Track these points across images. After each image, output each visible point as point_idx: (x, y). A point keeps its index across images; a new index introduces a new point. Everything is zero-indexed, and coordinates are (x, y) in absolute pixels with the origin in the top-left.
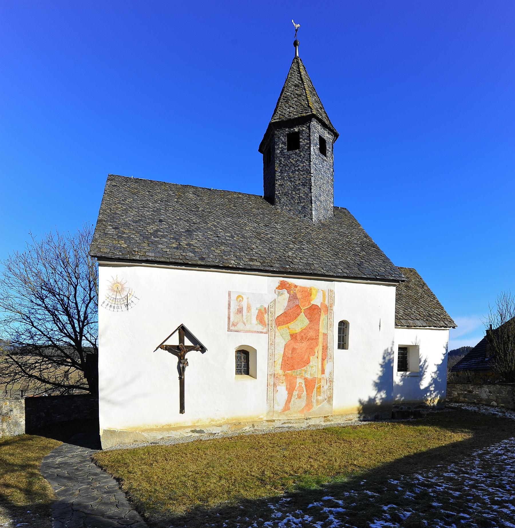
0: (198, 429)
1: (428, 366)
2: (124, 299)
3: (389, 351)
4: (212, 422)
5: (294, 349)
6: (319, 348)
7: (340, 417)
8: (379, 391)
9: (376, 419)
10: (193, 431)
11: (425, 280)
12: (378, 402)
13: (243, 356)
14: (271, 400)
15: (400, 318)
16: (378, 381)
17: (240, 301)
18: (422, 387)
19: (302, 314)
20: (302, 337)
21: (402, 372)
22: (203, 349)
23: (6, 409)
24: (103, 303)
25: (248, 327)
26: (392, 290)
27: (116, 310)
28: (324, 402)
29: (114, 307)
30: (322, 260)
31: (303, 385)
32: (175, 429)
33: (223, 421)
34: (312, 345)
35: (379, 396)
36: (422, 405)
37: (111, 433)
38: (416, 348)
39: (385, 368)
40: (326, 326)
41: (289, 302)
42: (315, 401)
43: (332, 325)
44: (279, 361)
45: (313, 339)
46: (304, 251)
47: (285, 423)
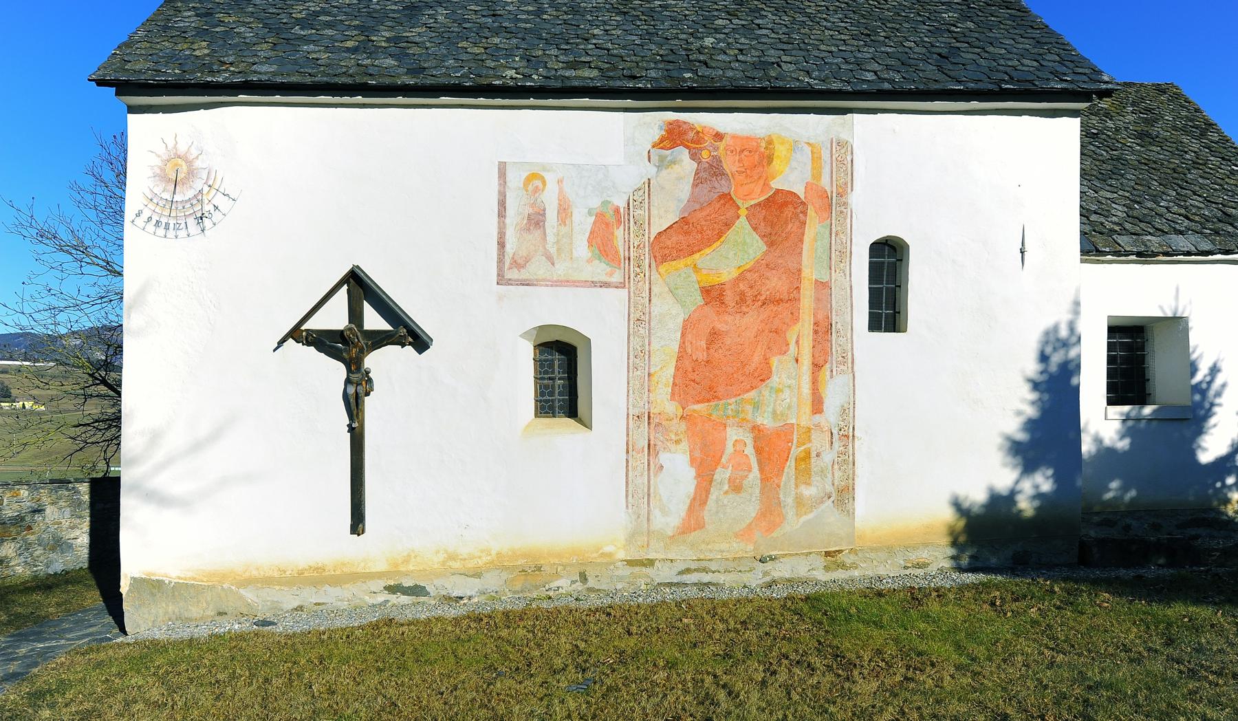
0: (407, 583)
1: (1224, 386)
2: (194, 202)
3: (1064, 333)
4: (451, 563)
5: (714, 336)
6: (802, 331)
8: (1029, 467)
9: (1018, 565)
10: (392, 589)
11: (1210, 113)
12: (1025, 505)
13: (557, 358)
14: (640, 496)
15: (1111, 230)
16: (1021, 436)
18: (1205, 457)
19: (742, 223)
20: (742, 294)
21: (1126, 408)
22: (420, 343)
23: (15, 506)
24: (138, 215)
25: (561, 270)
26: (1069, 129)
27: (171, 233)
28: (823, 507)
29: (167, 225)
30: (816, 53)
31: (750, 450)
32: (337, 580)
33: (486, 559)
34: (777, 322)
35: (1027, 486)
36: (1209, 516)
37: (151, 587)
38: (1176, 325)
39: (1048, 390)
40: (825, 257)
41: (695, 185)
42: (790, 501)
43: (846, 254)
44: (666, 373)
46: (760, 32)
47: (688, 571)
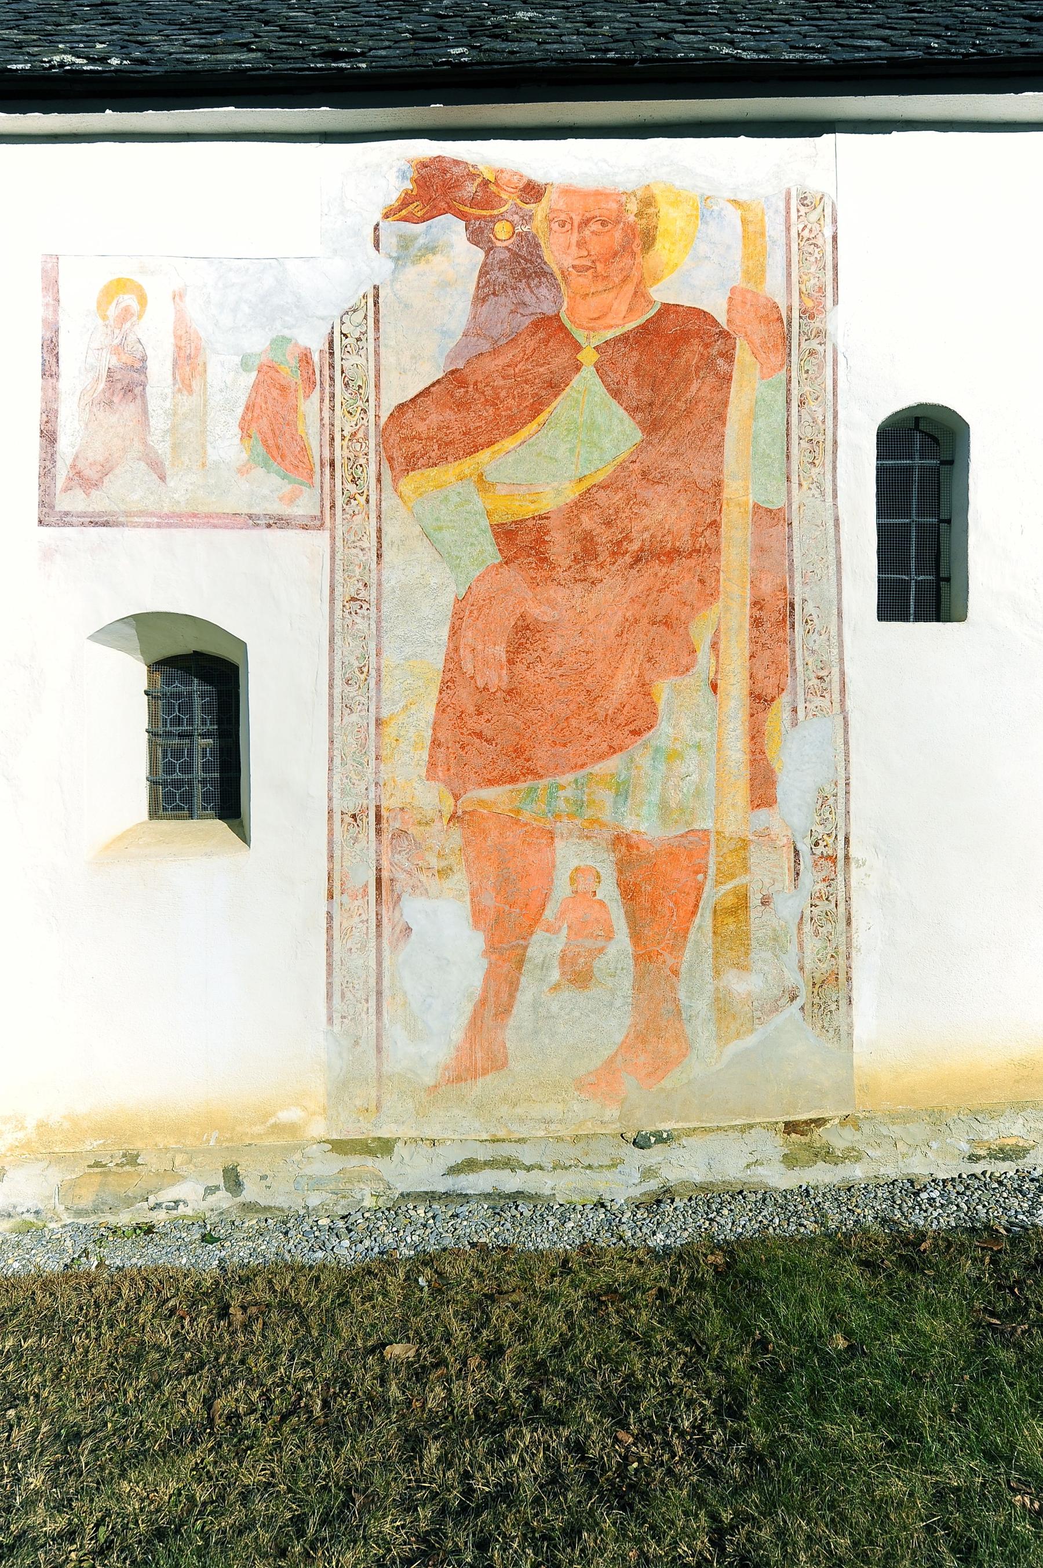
7: (918, 1130)
14: (359, 995)
17: (125, 315)
19: (587, 382)
31: (608, 891)
34: (667, 598)
40: (777, 453)
41: (480, 299)
42: (702, 1006)
43: (823, 448)
44: (417, 717)
45: (672, 555)
47: (470, 1165)
